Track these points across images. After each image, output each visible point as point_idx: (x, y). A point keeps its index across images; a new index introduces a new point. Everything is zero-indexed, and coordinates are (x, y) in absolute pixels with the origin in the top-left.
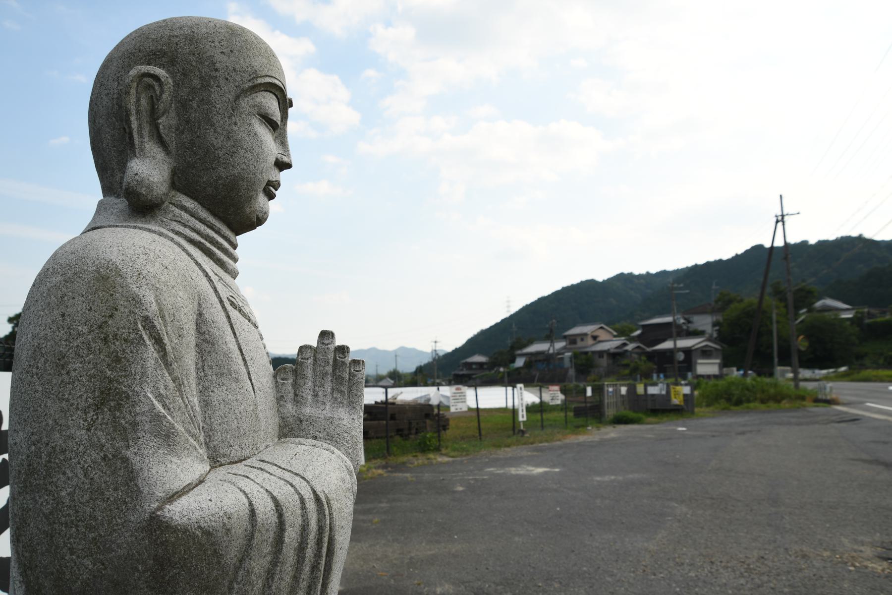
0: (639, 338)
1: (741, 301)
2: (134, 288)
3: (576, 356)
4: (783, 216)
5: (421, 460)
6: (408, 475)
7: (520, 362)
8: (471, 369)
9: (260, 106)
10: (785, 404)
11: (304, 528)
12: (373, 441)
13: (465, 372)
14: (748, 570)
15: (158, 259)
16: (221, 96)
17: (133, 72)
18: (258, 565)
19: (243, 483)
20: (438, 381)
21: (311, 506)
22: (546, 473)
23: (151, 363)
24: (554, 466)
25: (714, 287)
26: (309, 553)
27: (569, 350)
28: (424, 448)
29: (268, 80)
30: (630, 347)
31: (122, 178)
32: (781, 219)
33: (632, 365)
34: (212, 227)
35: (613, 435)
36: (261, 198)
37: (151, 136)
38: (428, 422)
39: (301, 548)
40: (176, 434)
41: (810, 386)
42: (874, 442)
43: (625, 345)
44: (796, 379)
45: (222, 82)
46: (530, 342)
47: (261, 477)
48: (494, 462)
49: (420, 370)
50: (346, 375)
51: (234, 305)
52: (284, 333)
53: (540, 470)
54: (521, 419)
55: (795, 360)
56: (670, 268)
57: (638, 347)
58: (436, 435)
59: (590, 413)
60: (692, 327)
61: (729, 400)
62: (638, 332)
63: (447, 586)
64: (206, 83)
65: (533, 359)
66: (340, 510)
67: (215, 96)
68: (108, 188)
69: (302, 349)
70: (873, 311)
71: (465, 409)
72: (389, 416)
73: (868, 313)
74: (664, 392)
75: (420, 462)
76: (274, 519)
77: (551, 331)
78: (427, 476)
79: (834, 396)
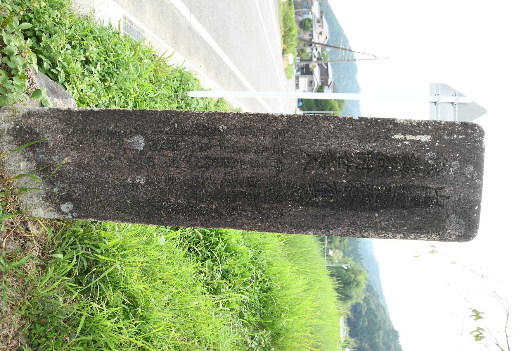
3: (310, 20)
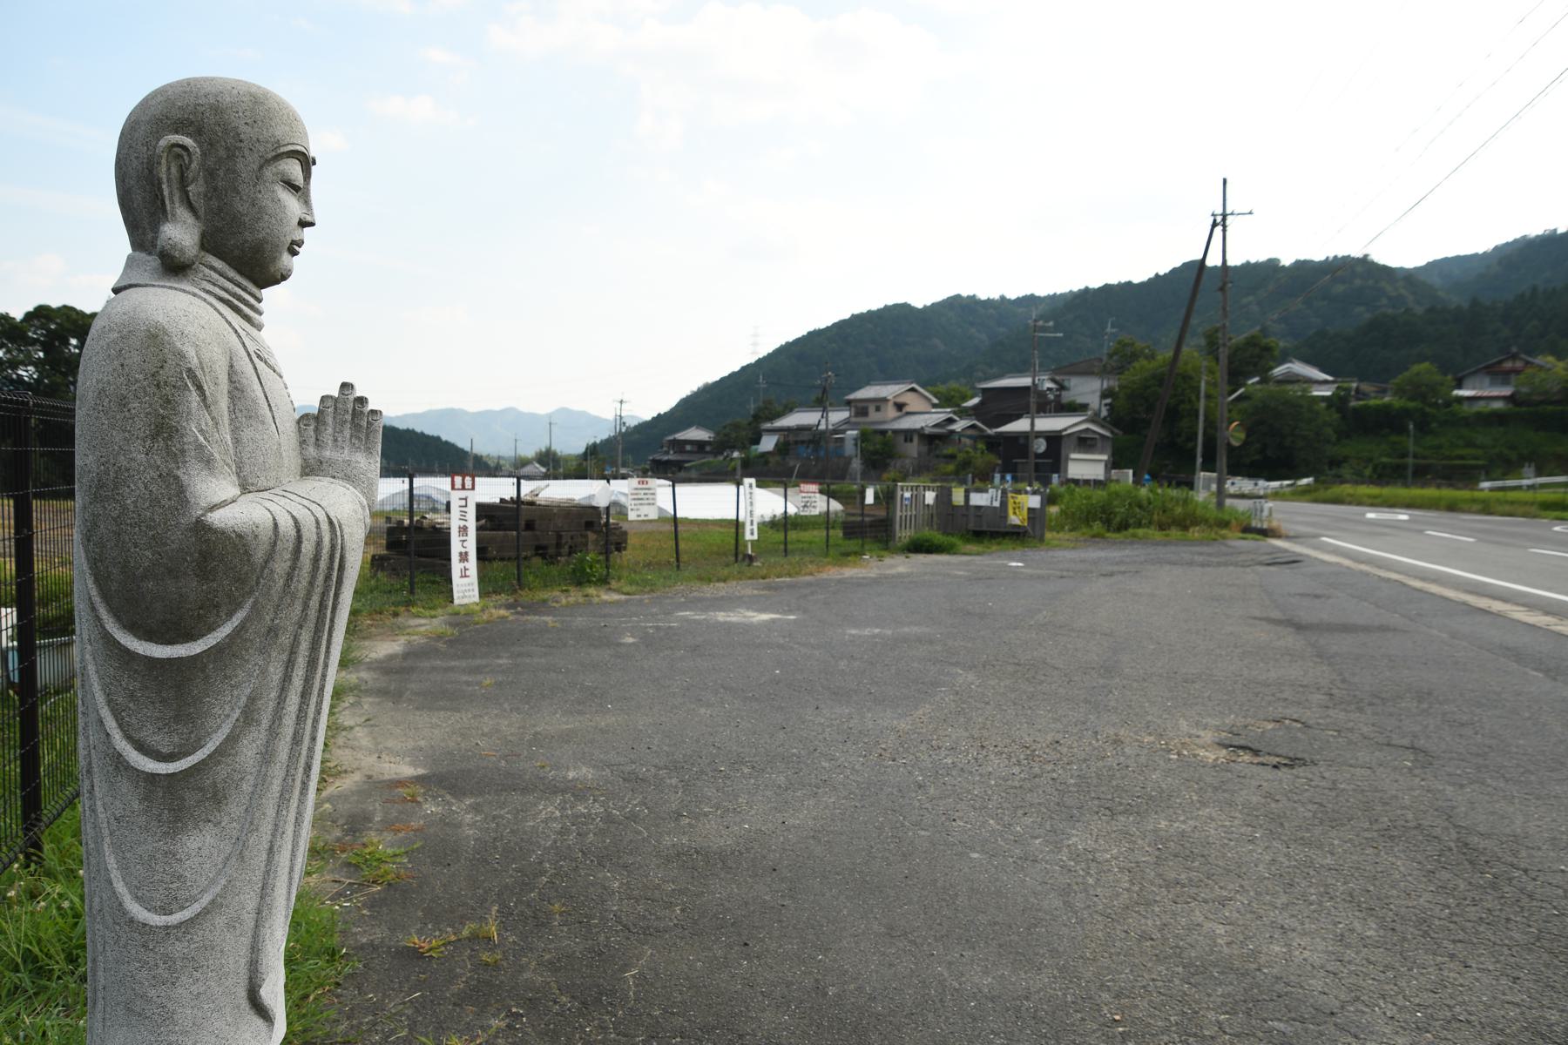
0: (975, 412)
1: (1152, 357)
2: (178, 345)
3: (864, 437)
4: (1224, 216)
5: (575, 596)
6: (548, 619)
7: (768, 444)
8: (682, 451)
9: (283, 174)
10: (1195, 533)
11: (319, 544)
12: (495, 564)
13: (671, 457)
14: (1031, 757)
15: (189, 313)
16: (246, 165)
17: (163, 143)
18: (281, 566)
19: (268, 504)
20: (623, 471)
21: (325, 526)
22: (773, 621)
23: (194, 405)
24: (790, 612)
25: (1109, 330)
26: (323, 564)
27: (853, 426)
28: (581, 578)
29: (291, 148)
30: (960, 425)
31: (156, 238)
32: (1220, 222)
33: (961, 456)
34: (239, 285)
35: (901, 569)
36: (286, 256)
37: (181, 201)
38: (591, 536)
39: (316, 559)
40: (214, 460)
41: (1242, 505)
42: (1302, 595)
43: (950, 421)
44: (1221, 494)
45: (247, 152)
46: (788, 409)
47: (283, 501)
48: (692, 603)
49: (593, 451)
50: (365, 424)
51: (259, 357)
52: (305, 388)
53: (765, 617)
54: (748, 537)
55: (1222, 461)
56: (1042, 291)
57: (973, 427)
58: (601, 558)
59: (869, 532)
60: (1067, 397)
61: (1107, 523)
62: (976, 401)
63: (584, 770)
64: (232, 154)
65: (792, 438)
66: (351, 534)
67: (240, 166)
68: (137, 244)
69: (324, 399)
70: (1365, 387)
71: (653, 515)
72: (522, 523)
73: (1357, 390)
74: (997, 504)
75: (572, 600)
76: (293, 533)
77: (824, 391)
78: (580, 621)
79: (1275, 524)
